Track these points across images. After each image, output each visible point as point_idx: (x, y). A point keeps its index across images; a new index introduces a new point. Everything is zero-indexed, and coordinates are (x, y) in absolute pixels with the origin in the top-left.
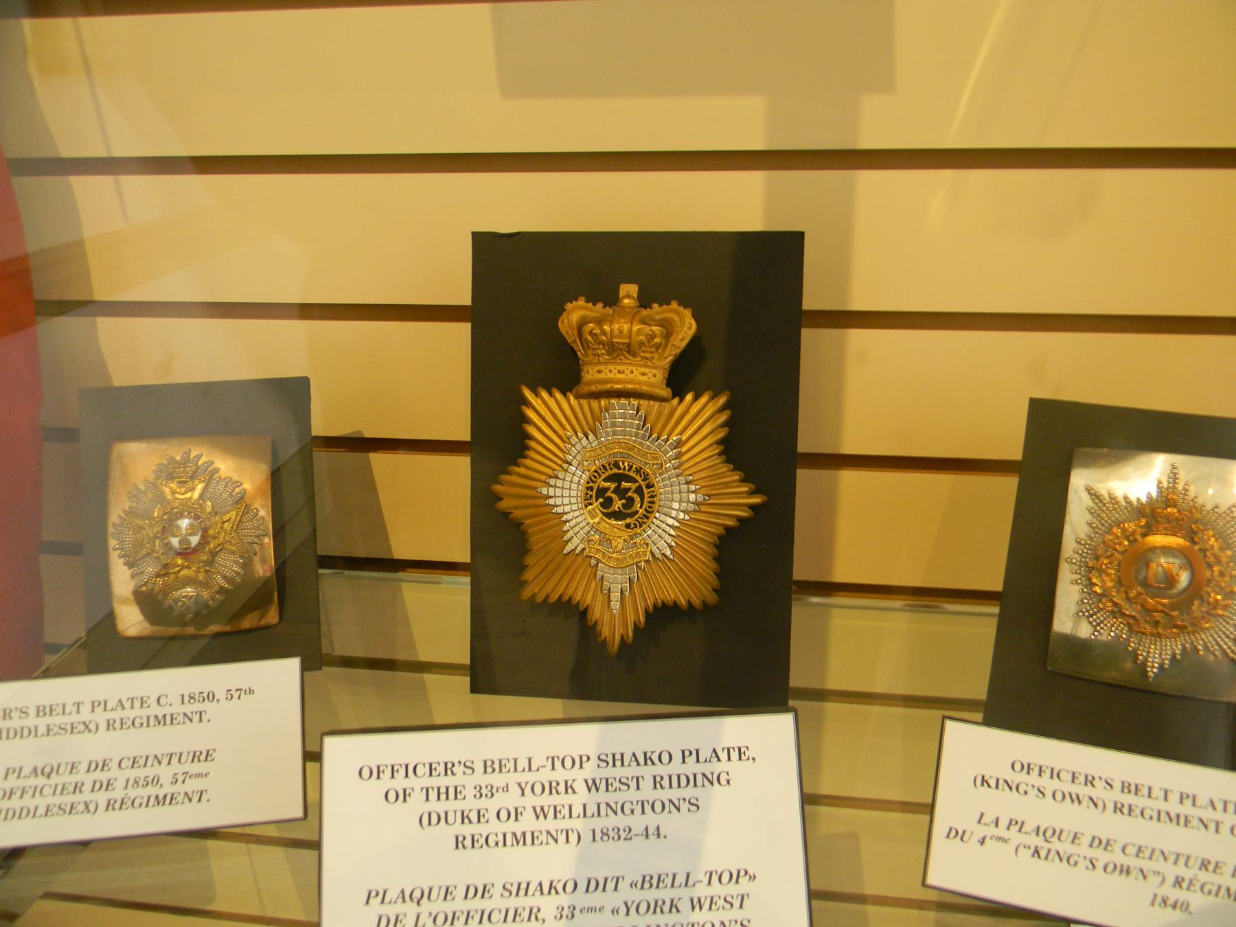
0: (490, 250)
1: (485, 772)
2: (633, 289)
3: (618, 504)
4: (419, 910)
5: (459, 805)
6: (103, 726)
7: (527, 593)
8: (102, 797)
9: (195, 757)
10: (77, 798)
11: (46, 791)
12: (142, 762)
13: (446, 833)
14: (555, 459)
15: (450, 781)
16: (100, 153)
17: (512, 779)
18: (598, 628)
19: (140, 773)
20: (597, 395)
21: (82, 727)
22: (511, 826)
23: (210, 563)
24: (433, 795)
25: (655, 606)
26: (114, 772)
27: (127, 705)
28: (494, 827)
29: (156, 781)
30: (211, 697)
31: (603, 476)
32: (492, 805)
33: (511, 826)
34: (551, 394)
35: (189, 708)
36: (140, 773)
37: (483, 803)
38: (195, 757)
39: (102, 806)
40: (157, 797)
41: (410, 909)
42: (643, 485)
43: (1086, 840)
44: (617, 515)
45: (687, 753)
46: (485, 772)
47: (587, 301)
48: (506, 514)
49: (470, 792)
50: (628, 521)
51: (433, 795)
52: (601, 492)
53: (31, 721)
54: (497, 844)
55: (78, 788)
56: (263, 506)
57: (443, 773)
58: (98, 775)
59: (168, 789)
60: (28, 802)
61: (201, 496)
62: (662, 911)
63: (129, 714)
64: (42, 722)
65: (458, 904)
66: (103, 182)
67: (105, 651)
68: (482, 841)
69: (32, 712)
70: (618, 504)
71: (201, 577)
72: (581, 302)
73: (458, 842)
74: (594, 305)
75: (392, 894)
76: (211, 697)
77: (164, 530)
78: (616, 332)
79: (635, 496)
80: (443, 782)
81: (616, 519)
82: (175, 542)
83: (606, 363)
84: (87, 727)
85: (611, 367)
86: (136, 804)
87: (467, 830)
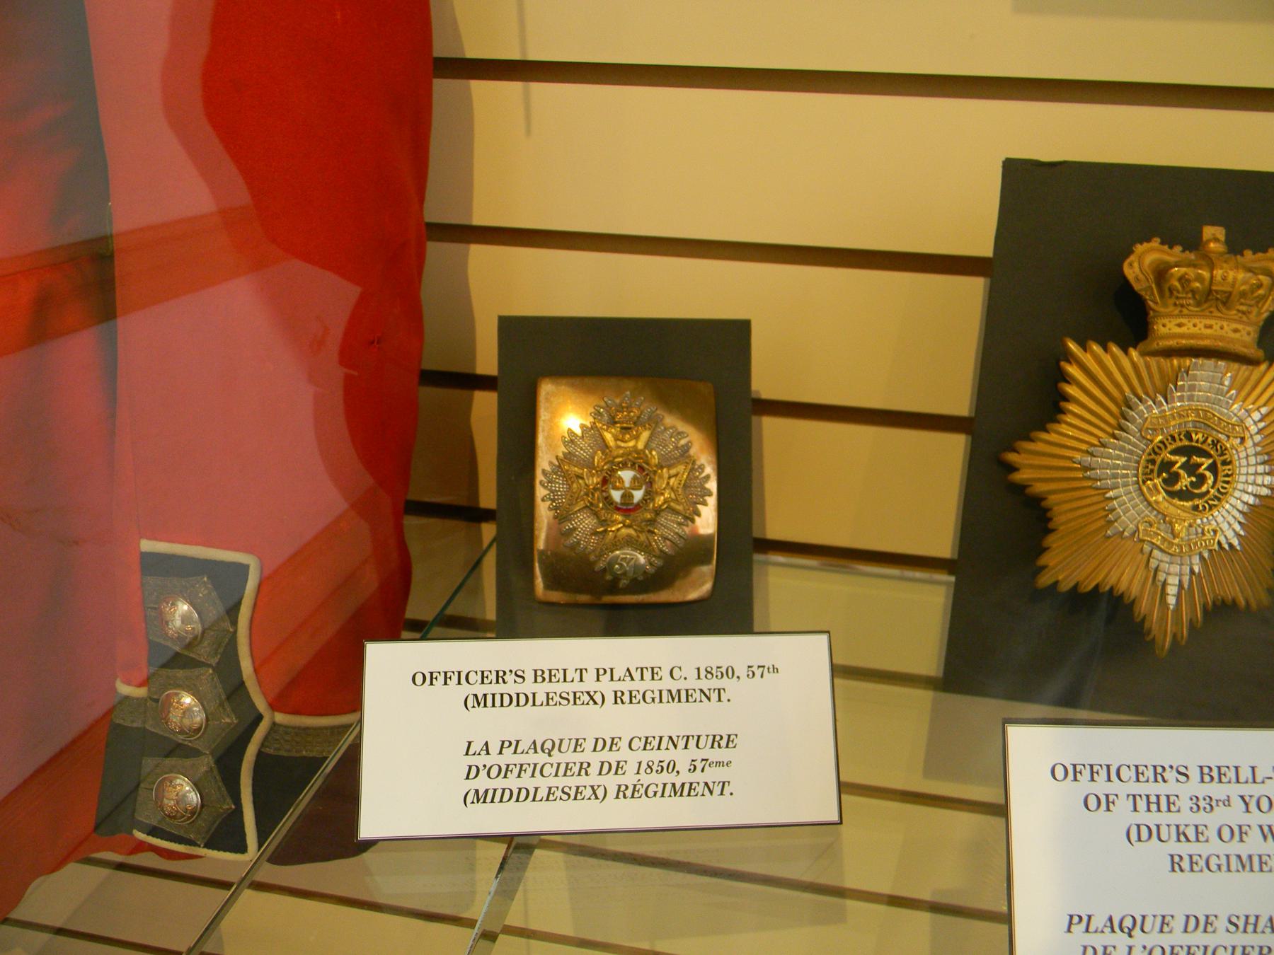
0: (1022, 178)
1: (1202, 781)
2: (1220, 232)
3: (1185, 481)
4: (1130, 942)
5: (1173, 818)
6: (610, 698)
7: (1044, 580)
8: (611, 782)
9: (715, 741)
10: (583, 780)
11: (547, 770)
12: (655, 743)
13: (1156, 853)
14: (1103, 425)
15: (1161, 789)
16: (515, 55)
17: (1234, 790)
18: (1147, 625)
19: (655, 756)
20: (1169, 353)
21: (586, 698)
22: (1235, 848)
23: (652, 522)
24: (1142, 804)
25: (1214, 603)
26: (623, 754)
27: (637, 675)
28: (1214, 847)
29: (672, 767)
30: (730, 672)
31: (1170, 448)
32: (1212, 820)
33: (1235, 848)
34: (1106, 349)
35: (705, 684)
36: (655, 756)
37: (1201, 818)
38: (715, 741)
39: (612, 792)
40: (674, 785)
41: (1121, 940)
42: (1219, 460)
43: (1178, 924)
44: (1184, 495)
45: (601, 672)
46: (1202, 781)
47: (1162, 243)
48: (1020, 489)
49: (1184, 803)
50: (1196, 502)
51: (1142, 804)
52: (1167, 466)
53: (528, 687)
54: (653, 699)
55: (584, 768)
56: (709, 463)
57: (1152, 778)
58: (606, 755)
59: (686, 777)
60: (527, 782)
61: (646, 446)
62: (625, 797)
63: (638, 685)
64: (541, 689)
65: (1177, 938)
66: (511, 89)
67: (235, 632)
68: (640, 697)
69: (529, 676)
70: (1185, 481)
71: (643, 537)
72: (1155, 243)
73: (1175, 864)
74: (1171, 247)
75: (1098, 922)
76: (730, 672)
77: (605, 481)
78: (1219, 278)
79: (1208, 474)
80: (1153, 789)
81: (1181, 499)
82: (616, 495)
83: (1188, 316)
84: (592, 698)
85: (1196, 321)
86: (650, 793)
87: (1184, 849)
